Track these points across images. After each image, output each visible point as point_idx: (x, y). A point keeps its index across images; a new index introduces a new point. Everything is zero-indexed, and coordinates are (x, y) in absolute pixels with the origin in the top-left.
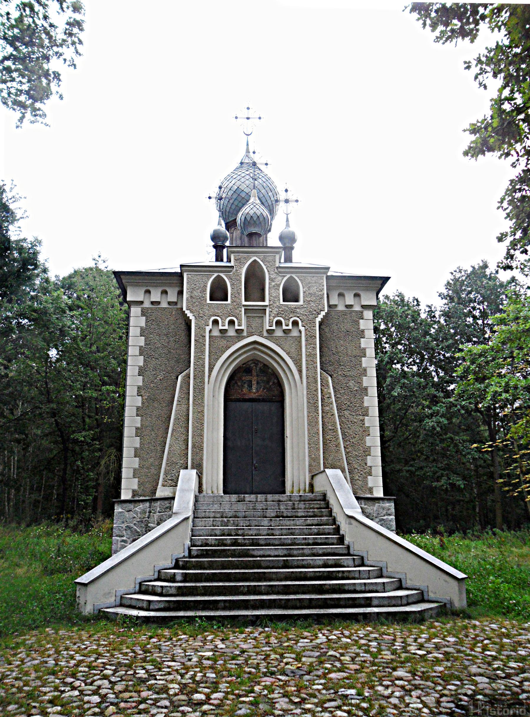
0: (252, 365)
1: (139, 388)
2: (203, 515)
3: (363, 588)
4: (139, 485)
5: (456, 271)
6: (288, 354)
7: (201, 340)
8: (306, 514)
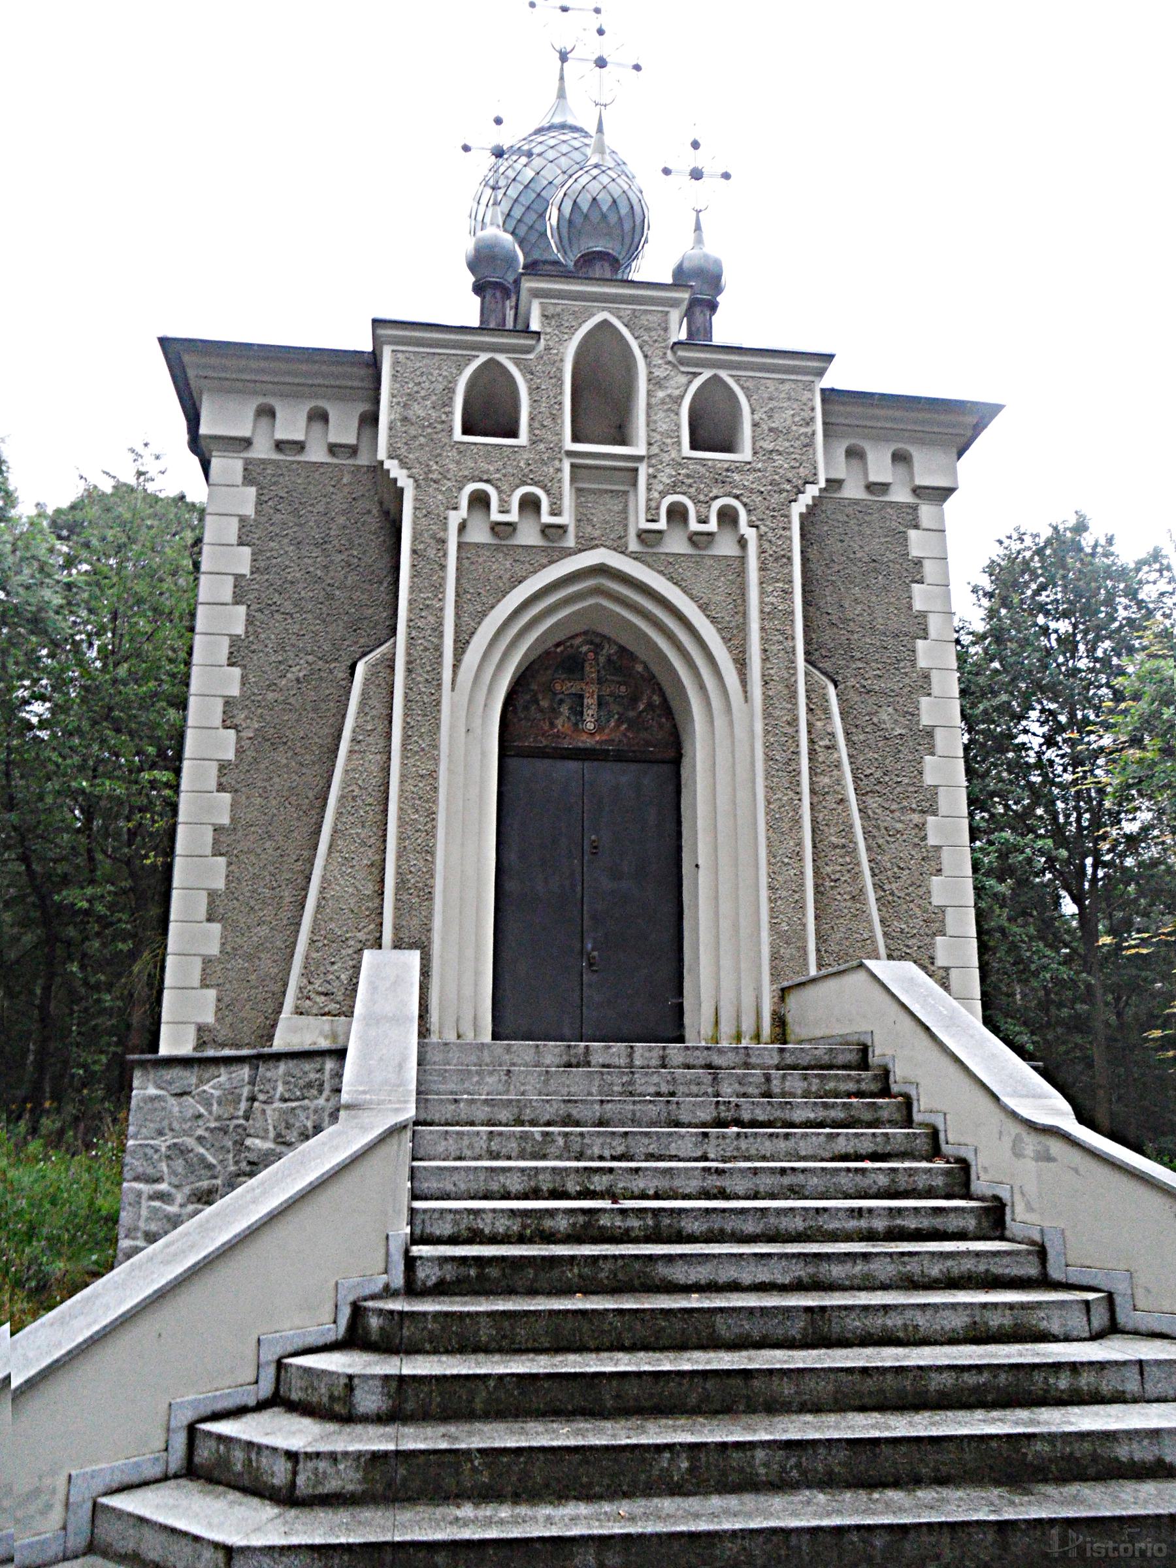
1: (228, 702)
2: (449, 1111)
4: (218, 1010)
5: (1010, 537)
6: (704, 608)
7: (431, 553)
8: (821, 1114)
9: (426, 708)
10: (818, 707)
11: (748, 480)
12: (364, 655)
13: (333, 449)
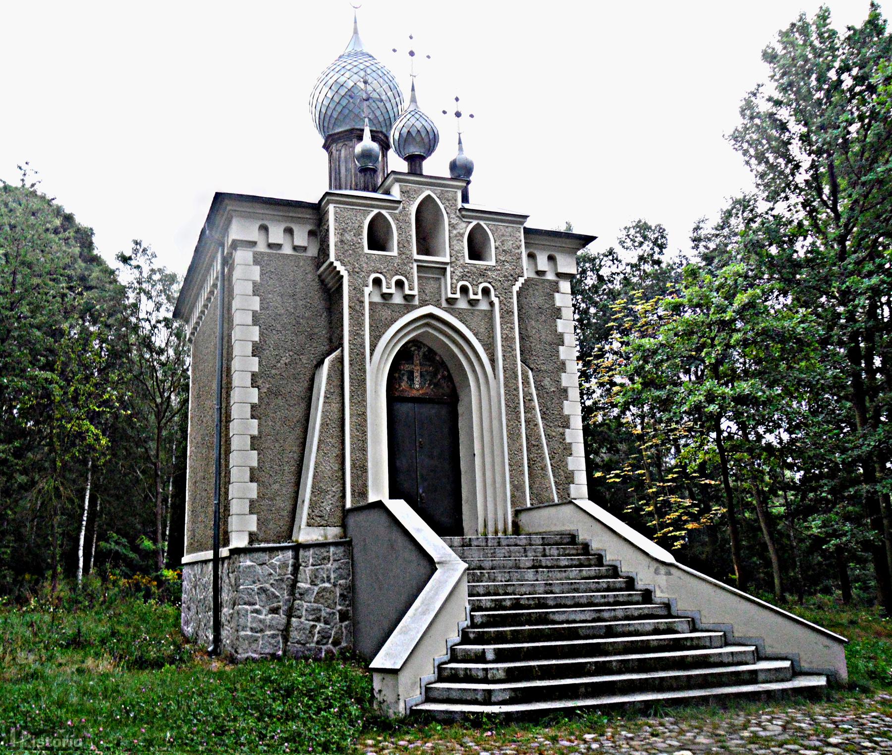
0: (413, 349)
1: (254, 375)
3: (730, 659)
6: (476, 335)
7: (358, 308)
9: (360, 382)
10: (526, 382)
11: (493, 275)
12: (328, 355)
13: (295, 248)
